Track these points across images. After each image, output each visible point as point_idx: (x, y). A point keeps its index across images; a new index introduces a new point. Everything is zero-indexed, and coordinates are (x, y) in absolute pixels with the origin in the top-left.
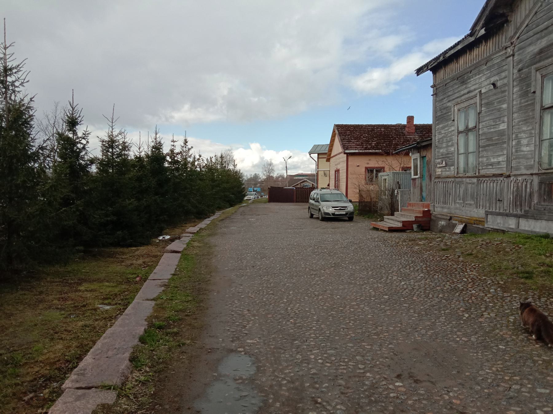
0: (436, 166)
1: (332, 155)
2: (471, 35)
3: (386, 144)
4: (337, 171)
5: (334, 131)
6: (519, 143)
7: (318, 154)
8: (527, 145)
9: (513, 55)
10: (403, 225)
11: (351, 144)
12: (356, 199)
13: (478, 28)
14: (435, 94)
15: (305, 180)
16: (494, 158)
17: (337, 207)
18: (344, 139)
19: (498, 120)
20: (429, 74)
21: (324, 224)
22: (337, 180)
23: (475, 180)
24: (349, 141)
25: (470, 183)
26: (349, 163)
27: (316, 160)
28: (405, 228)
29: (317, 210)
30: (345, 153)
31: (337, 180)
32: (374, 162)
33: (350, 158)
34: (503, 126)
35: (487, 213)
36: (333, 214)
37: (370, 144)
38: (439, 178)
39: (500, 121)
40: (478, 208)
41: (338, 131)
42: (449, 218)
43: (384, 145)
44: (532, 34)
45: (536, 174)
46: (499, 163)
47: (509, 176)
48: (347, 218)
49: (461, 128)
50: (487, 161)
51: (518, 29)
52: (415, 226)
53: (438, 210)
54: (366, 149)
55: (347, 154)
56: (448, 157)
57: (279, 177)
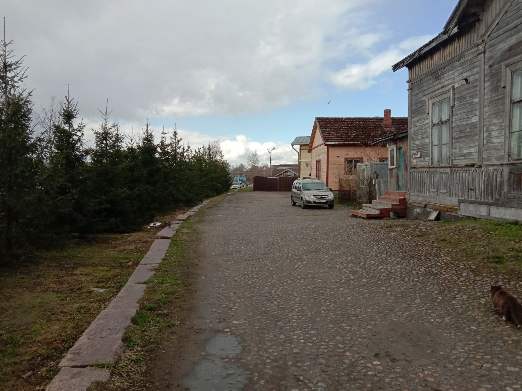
0: (411, 157)
1: (313, 147)
2: (444, 33)
3: (365, 136)
4: (318, 162)
5: (315, 124)
6: (490, 135)
7: (301, 146)
8: (498, 137)
9: (484, 52)
10: (380, 213)
11: (332, 136)
12: (336, 188)
13: (451, 26)
14: (411, 89)
15: (288, 170)
16: (466, 149)
17: (318, 196)
18: (324, 132)
19: (470, 114)
20: (405, 70)
21: (306, 211)
22: (318, 170)
23: (448, 170)
24: (330, 134)
25: (444, 173)
26: (330, 154)
27: (299, 151)
28: (383, 216)
29: (299, 198)
30: (326, 145)
31: (318, 170)
32: (353, 153)
33: (331, 150)
34: (475, 119)
35: (460, 202)
36: (315, 202)
37: (349, 136)
38: (414, 168)
39: (472, 114)
40: (452, 196)
41: (319, 123)
42: (423, 206)
43: (363, 137)
44: (503, 33)
45: (506, 164)
46: (471, 154)
47: (480, 166)
48: (327, 206)
49: (436, 121)
50: (460, 152)
51: (489, 27)
52: (392, 214)
53: (413, 198)
54: (345, 140)
55: (327, 145)
56: (423, 149)
57: (263, 167)
